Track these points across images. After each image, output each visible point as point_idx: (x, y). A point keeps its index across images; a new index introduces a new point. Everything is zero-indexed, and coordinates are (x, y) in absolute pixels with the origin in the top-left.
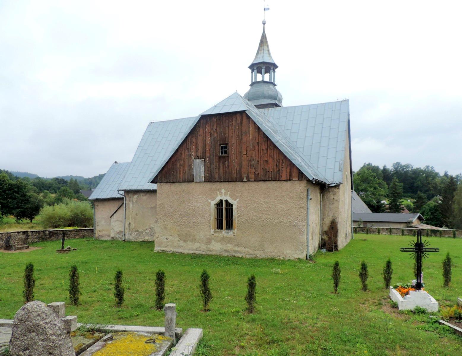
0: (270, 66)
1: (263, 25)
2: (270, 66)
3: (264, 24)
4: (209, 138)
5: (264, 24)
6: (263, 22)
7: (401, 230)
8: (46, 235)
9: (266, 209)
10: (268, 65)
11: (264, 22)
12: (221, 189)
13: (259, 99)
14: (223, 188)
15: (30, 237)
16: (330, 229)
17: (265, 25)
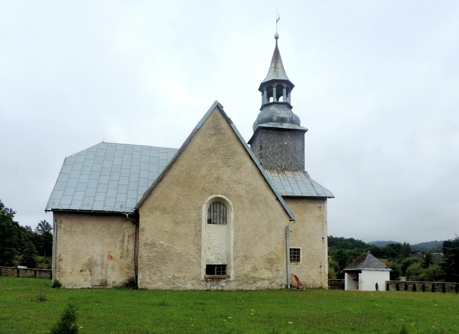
1: (275, 40)
3: (277, 38)
5: (277, 38)
17: (278, 40)
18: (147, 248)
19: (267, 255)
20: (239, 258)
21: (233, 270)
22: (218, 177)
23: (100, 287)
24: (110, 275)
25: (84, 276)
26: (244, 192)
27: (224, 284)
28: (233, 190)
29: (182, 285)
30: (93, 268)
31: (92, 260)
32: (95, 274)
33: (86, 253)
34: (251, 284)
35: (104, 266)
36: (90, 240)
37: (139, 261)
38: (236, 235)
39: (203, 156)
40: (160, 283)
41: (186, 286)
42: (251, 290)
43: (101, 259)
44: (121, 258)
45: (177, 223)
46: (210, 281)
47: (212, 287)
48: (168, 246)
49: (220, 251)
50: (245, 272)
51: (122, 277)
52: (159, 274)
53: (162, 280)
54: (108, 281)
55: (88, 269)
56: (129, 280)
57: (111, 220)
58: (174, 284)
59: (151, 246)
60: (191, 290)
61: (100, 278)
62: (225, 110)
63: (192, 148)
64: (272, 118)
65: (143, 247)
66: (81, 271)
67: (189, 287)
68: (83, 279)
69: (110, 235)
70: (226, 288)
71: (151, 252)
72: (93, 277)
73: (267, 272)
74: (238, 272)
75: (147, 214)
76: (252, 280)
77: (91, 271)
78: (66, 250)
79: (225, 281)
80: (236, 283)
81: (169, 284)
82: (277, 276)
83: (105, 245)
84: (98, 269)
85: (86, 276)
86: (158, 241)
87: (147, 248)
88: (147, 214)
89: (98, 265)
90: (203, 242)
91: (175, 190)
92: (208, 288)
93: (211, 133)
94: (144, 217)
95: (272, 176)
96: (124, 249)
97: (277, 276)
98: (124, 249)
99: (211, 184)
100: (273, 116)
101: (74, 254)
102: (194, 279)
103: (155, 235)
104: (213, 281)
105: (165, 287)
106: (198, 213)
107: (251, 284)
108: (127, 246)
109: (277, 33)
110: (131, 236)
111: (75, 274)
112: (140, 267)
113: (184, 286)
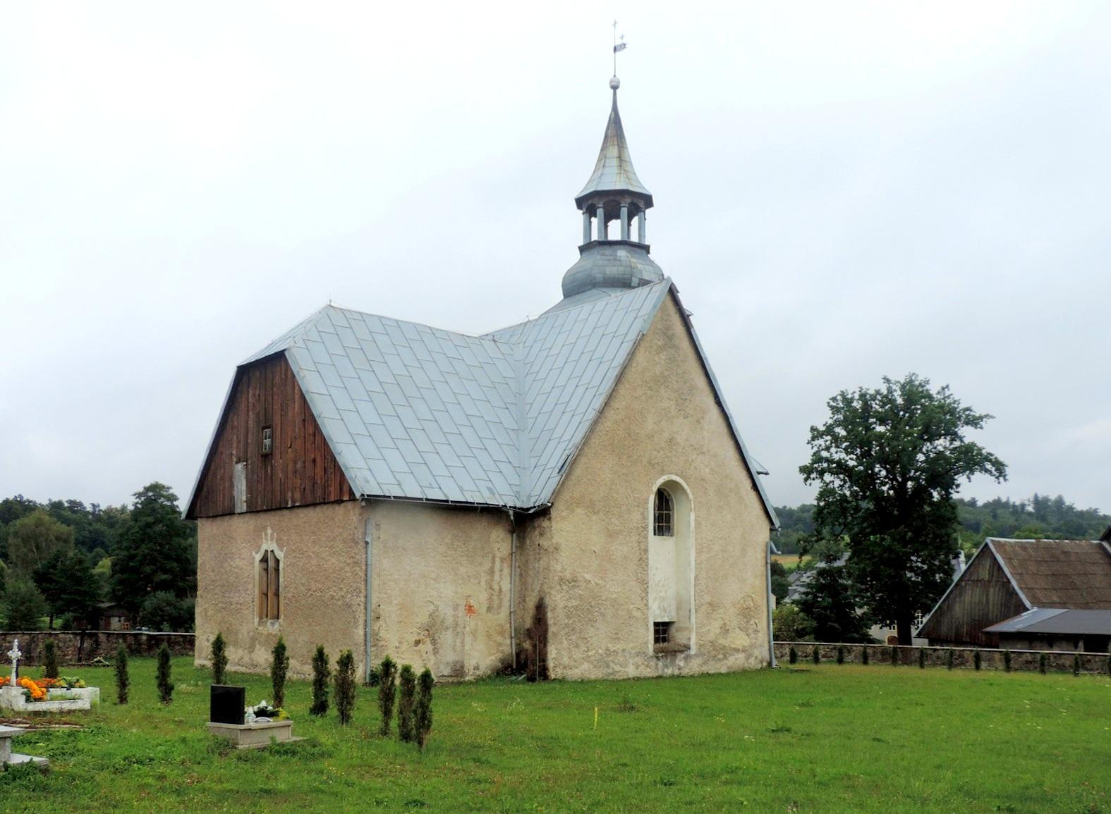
0: (618, 198)
1: (612, 91)
2: (618, 198)
3: (615, 88)
4: (251, 415)
5: (615, 88)
6: (611, 82)
7: (1073, 657)
8: (141, 644)
9: (315, 569)
10: (612, 198)
11: (614, 84)
12: (265, 528)
13: (584, 291)
14: (269, 524)
15: (104, 645)
16: (535, 624)
17: (618, 91)
18: (564, 588)
19: (742, 601)
20: (703, 609)
21: (694, 634)
22: (670, 437)
23: (450, 680)
24: (470, 650)
25: (421, 656)
26: (707, 470)
27: (682, 664)
28: (692, 467)
29: (621, 669)
30: (438, 634)
31: (437, 616)
32: (442, 648)
33: (425, 599)
34: (719, 660)
35: (459, 630)
36: (433, 569)
37: (552, 618)
38: (699, 560)
39: (649, 393)
40: (586, 666)
41: (626, 670)
42: (708, 674)
43: (453, 613)
44: (489, 609)
45: (611, 535)
46: (662, 657)
47: (666, 670)
48: (598, 584)
49: (666, 591)
50: (711, 637)
51: (490, 654)
52: (584, 645)
53: (587, 659)
54: (466, 665)
55: (430, 637)
56: (502, 661)
57: (470, 522)
58: (608, 666)
59: (570, 585)
60: (634, 678)
61: (450, 657)
62: (682, 297)
63: (632, 374)
64: (631, 280)
65: (558, 587)
66: (417, 643)
67: (632, 672)
68: (421, 662)
69: (468, 557)
70: (685, 672)
71: (570, 597)
72: (438, 656)
73: (743, 635)
74: (702, 637)
75: (564, 514)
76: (721, 652)
77: (434, 642)
78: (387, 594)
79: (683, 656)
80: (699, 661)
81: (600, 666)
82: (755, 643)
83: (460, 582)
84: (447, 638)
85: (425, 655)
86: (580, 572)
87: (564, 588)
88: (564, 514)
89: (447, 628)
90: (651, 573)
91: (607, 462)
92: (660, 672)
93: (660, 343)
94: (559, 519)
95: (319, 332)
96: (493, 590)
97: (755, 643)
98: (493, 590)
99: (661, 453)
100: (632, 275)
101: (403, 603)
102: (638, 654)
103: (576, 561)
104: (666, 656)
105: (595, 674)
106: (642, 514)
107: (719, 660)
108: (500, 582)
109: (615, 76)
110: (505, 559)
111: (404, 651)
112: (553, 632)
113: (623, 669)
